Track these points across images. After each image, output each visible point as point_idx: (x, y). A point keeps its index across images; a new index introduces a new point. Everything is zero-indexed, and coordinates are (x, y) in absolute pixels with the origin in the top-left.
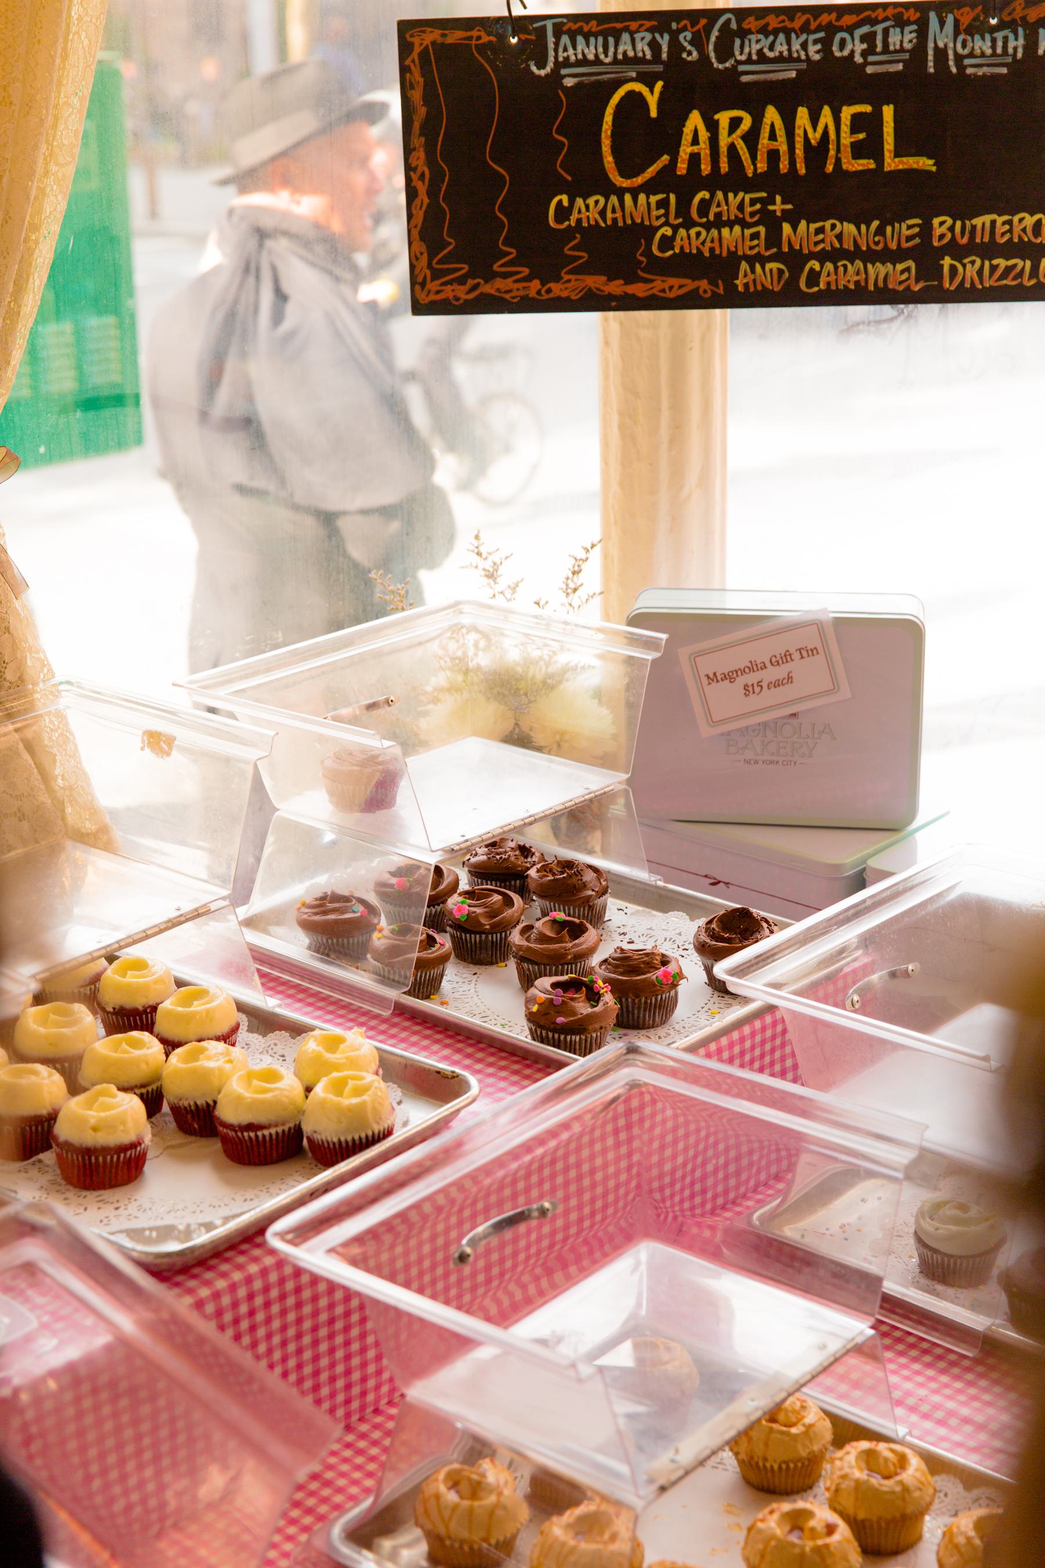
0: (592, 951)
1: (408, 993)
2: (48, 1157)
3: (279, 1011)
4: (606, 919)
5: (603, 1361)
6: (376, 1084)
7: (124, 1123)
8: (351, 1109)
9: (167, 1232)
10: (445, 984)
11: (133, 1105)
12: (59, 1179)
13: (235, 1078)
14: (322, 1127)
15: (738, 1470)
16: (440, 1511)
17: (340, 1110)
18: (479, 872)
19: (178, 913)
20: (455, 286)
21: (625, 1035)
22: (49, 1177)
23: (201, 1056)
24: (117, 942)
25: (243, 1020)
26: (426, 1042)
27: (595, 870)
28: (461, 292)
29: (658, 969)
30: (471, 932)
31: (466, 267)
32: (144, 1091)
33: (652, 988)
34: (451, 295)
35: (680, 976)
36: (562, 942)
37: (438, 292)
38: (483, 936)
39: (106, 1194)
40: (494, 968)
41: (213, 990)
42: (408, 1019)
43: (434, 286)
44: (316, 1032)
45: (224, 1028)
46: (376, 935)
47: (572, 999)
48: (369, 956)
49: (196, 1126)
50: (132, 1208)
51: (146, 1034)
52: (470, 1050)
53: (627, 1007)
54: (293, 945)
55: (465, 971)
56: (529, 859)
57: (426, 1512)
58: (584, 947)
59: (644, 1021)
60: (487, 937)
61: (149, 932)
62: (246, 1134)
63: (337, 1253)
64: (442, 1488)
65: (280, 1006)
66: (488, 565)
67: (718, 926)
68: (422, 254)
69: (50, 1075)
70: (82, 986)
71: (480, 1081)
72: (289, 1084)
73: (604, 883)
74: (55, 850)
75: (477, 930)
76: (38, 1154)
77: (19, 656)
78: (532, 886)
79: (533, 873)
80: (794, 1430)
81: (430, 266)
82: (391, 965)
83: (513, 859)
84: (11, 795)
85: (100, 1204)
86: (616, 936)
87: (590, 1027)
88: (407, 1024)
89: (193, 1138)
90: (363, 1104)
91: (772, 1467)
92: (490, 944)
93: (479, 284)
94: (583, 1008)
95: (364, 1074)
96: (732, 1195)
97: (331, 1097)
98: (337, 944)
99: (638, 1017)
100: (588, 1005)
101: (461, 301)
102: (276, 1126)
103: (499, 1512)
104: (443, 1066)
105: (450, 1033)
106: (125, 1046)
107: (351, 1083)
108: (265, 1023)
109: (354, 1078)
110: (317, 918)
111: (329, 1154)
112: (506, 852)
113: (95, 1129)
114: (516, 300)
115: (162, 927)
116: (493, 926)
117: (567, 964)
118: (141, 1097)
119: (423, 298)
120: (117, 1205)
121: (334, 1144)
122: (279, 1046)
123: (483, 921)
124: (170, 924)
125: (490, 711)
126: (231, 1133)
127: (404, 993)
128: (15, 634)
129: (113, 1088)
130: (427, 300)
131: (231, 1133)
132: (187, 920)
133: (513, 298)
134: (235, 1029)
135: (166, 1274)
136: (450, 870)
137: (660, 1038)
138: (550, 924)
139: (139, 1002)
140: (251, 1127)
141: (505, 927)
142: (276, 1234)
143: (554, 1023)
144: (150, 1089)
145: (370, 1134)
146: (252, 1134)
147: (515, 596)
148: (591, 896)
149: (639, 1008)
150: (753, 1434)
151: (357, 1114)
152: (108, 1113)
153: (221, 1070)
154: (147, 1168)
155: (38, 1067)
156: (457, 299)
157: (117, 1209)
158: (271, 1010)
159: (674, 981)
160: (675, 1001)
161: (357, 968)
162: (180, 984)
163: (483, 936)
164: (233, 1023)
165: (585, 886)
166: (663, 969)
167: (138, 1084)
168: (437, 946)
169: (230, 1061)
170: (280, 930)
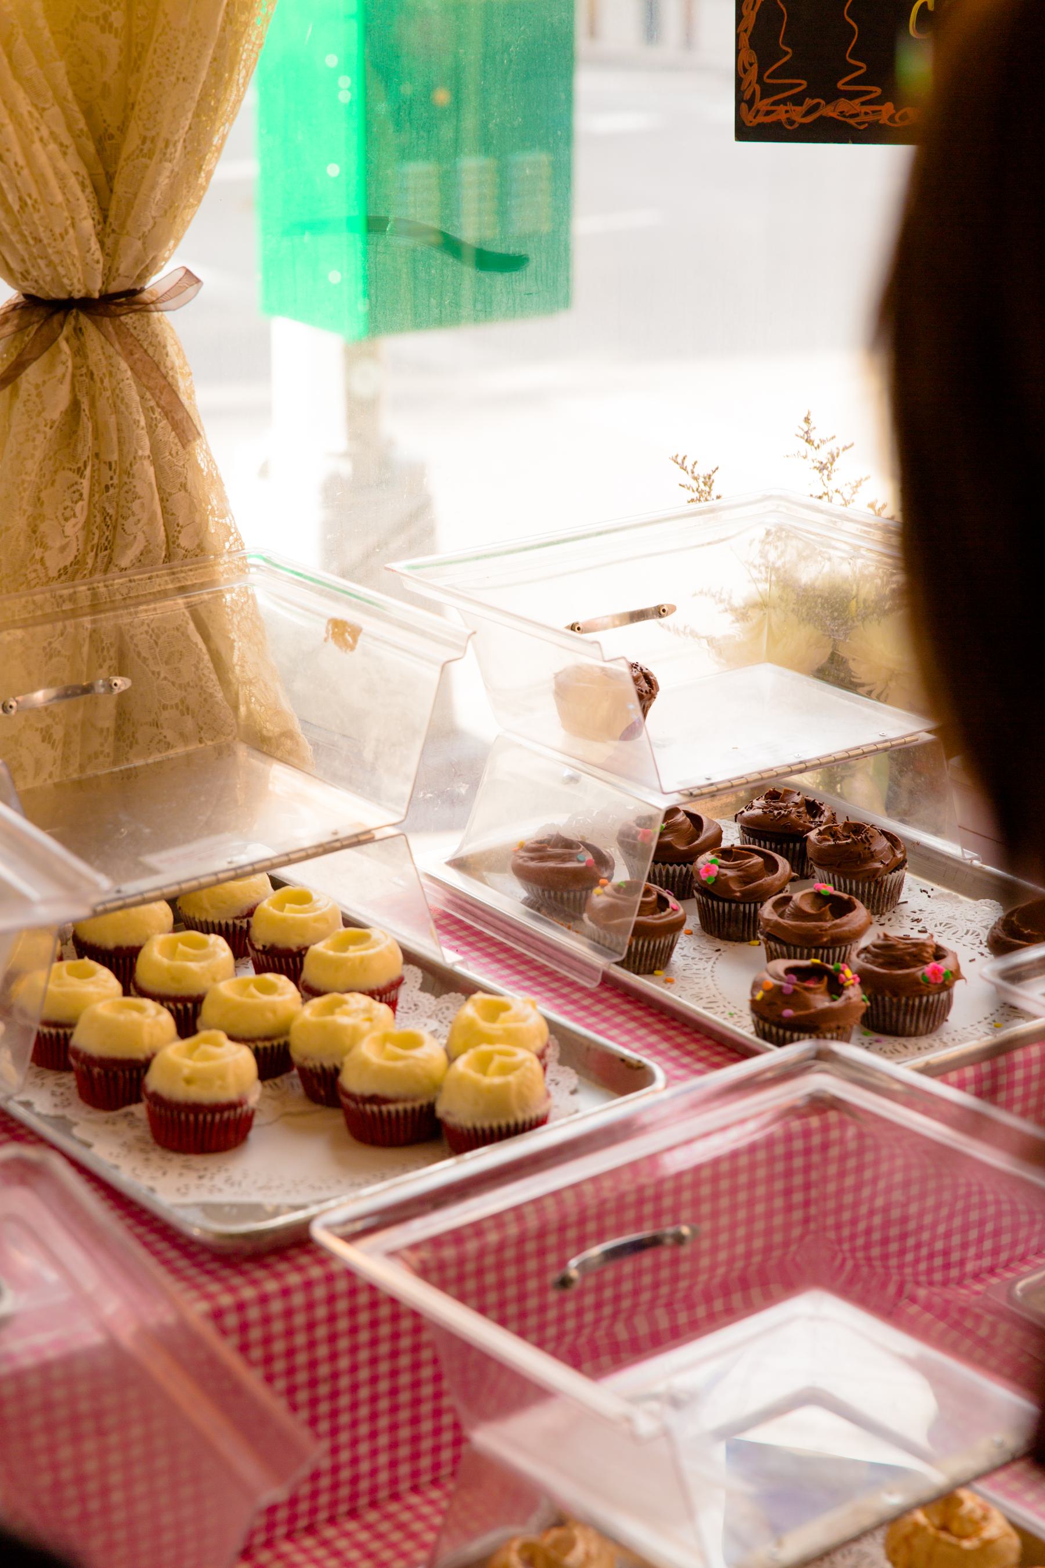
0: (858, 934)
1: (619, 964)
2: (139, 1110)
3: (460, 969)
4: (900, 901)
5: (758, 1435)
7: (222, 1077)
8: (492, 1090)
9: (255, 1210)
10: (676, 957)
11: (241, 1060)
12: (149, 1137)
14: (456, 1110)
17: (480, 1091)
18: (753, 829)
20: (790, 107)
21: (877, 1041)
22: (138, 1132)
23: (337, 1010)
24: (252, 864)
25: (414, 976)
27: (893, 839)
28: (797, 114)
29: (926, 963)
30: (719, 899)
31: (805, 83)
32: (261, 1045)
33: (916, 987)
34: (783, 117)
35: (956, 975)
36: (821, 920)
37: (768, 113)
38: (733, 906)
39: (196, 1160)
40: (744, 946)
42: (619, 996)
43: (763, 105)
44: (479, 996)
45: (381, 981)
46: (598, 890)
47: (807, 989)
48: (585, 916)
50: (219, 1180)
51: (284, 978)
52: (681, 1039)
53: (884, 1006)
54: (506, 897)
55: (707, 945)
56: (817, 820)
58: (846, 928)
59: (904, 1028)
60: (737, 907)
61: (293, 856)
65: (462, 963)
66: (823, 455)
67: (1018, 920)
68: (751, 65)
69: (159, 1013)
70: (237, 918)
71: (666, 1072)
73: (900, 856)
74: (223, 752)
75: (726, 897)
77: (197, 520)
78: (810, 851)
79: (813, 835)
80: (967, 1544)
81: (760, 80)
82: (606, 927)
83: (793, 816)
84: (173, 684)
85: (184, 1171)
86: (907, 923)
87: (823, 1026)
88: (616, 1001)
89: (318, 1107)
90: (506, 1087)
92: (741, 915)
93: (819, 104)
94: (821, 1002)
96: (1004, 1256)
97: (474, 1075)
98: (550, 897)
99: (897, 1021)
100: (827, 998)
101: (796, 126)
102: (405, 1100)
105: (665, 1017)
106: (253, 990)
107: (498, 1060)
108: (442, 982)
109: (501, 1053)
110: (533, 864)
111: (466, 1141)
112: (787, 807)
113: (188, 1081)
114: (862, 127)
115: (310, 852)
116: (744, 894)
117: (823, 948)
118: (257, 1053)
119: (751, 121)
120: (202, 1173)
122: (451, 1011)
123: (734, 886)
124: (320, 850)
125: (802, 637)
127: (617, 963)
128: (193, 492)
129: (222, 1036)
130: (756, 122)
131: (352, 1105)
132: (343, 847)
133: (860, 124)
134: (398, 983)
136: (711, 821)
137: (919, 1049)
138: (809, 900)
139: (293, 942)
140: (374, 1099)
141: (759, 897)
143: (780, 1016)
144: (275, 1043)
146: (375, 1108)
147: (855, 497)
148: (878, 869)
149: (898, 1009)
150: (916, 1542)
151: (498, 1098)
154: (253, 1134)
155: (148, 1003)
156: (791, 122)
157: (201, 1177)
158: (449, 967)
159: (946, 983)
160: (948, 1005)
161: (569, 928)
163: (733, 906)
164: (394, 976)
165: (872, 856)
166: (933, 964)
168: (669, 910)
169: (370, 1020)
170: (495, 877)
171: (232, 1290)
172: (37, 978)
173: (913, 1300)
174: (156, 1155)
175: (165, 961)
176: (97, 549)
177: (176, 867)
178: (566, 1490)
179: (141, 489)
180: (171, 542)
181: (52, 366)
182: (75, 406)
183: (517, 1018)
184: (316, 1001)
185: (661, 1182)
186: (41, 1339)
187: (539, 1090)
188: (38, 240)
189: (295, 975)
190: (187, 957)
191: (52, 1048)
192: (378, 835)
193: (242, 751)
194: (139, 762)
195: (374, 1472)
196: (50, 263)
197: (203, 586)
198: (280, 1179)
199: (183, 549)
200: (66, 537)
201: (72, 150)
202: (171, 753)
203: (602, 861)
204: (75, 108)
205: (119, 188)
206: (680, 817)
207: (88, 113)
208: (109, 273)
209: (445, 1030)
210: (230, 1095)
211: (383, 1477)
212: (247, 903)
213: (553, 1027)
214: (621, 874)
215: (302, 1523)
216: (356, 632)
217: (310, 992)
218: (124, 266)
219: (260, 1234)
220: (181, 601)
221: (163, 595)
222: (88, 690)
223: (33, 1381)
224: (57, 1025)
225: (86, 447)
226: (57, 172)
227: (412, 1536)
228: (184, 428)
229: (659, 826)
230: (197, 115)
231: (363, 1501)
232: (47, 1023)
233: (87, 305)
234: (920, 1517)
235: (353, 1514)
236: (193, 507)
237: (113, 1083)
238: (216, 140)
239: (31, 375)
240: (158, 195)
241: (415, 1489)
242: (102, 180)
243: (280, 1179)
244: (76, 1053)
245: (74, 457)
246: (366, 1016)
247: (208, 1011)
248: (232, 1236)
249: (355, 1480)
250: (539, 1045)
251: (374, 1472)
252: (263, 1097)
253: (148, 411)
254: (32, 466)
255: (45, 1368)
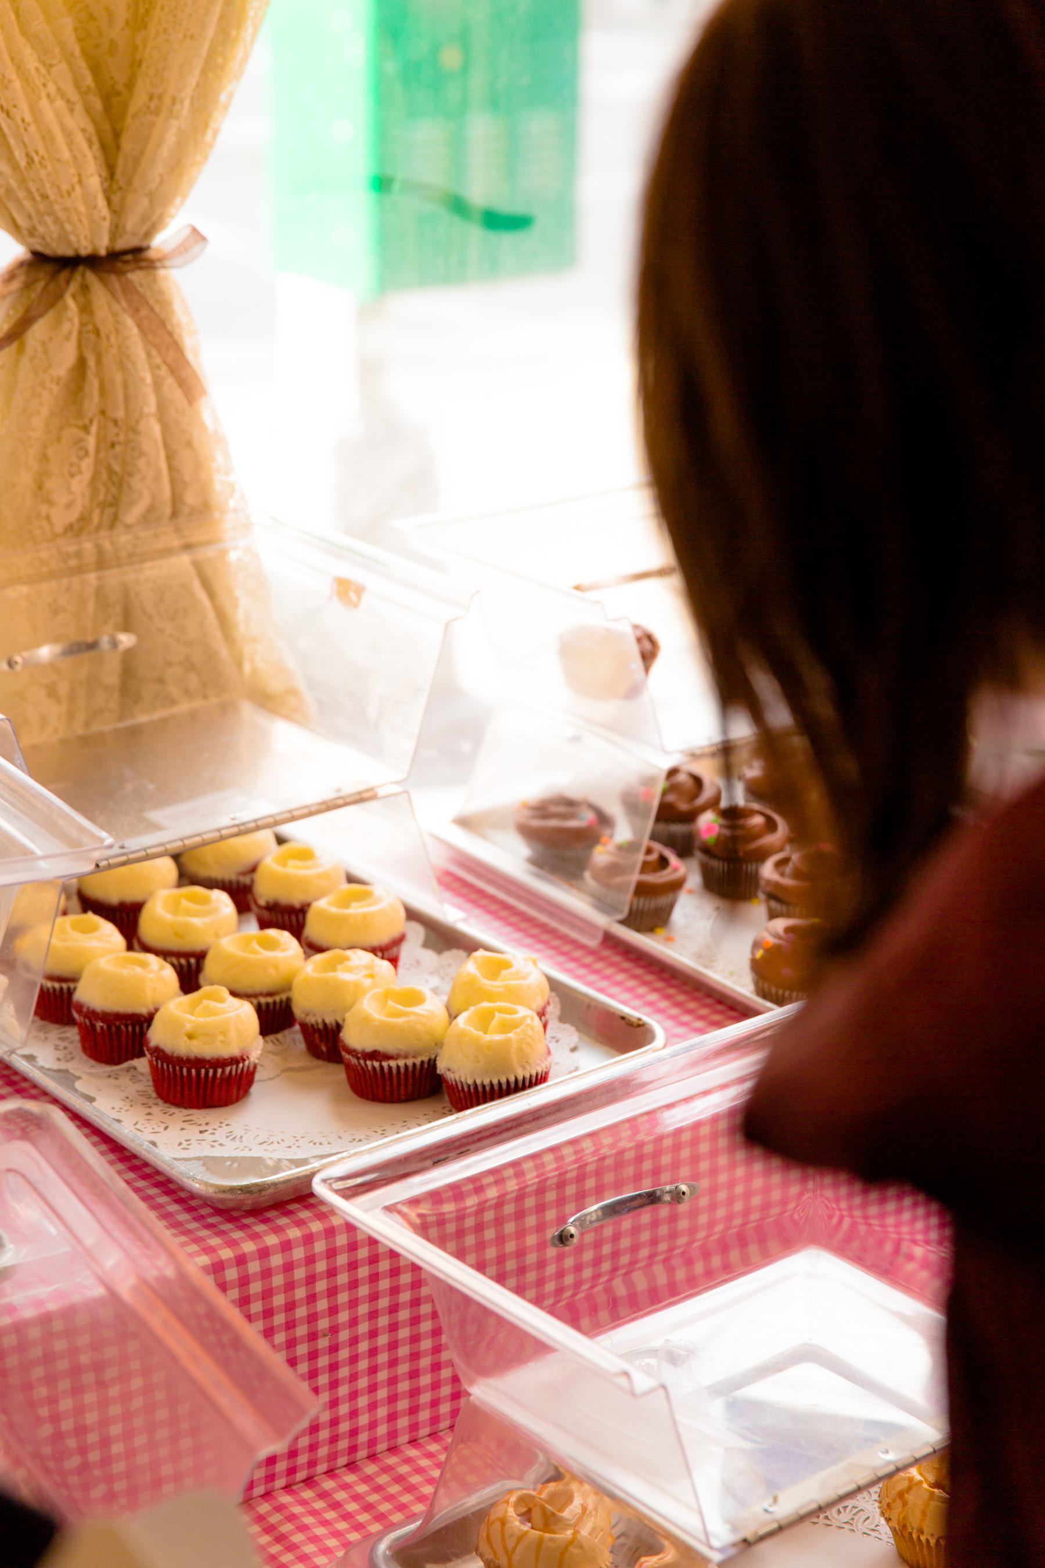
1: (622, 922)
2: (142, 1064)
6: (529, 1021)
7: (224, 1033)
8: (491, 1046)
11: (246, 1013)
13: (368, 996)
14: (457, 1067)
15: (892, 1541)
16: (503, 1539)
19: (337, 795)
22: (140, 1087)
23: (340, 967)
24: (255, 821)
25: (416, 933)
26: (632, 983)
32: (263, 1000)
39: (198, 1115)
41: (377, 890)
44: (480, 953)
45: (383, 938)
48: (587, 875)
49: (324, 1049)
50: (221, 1135)
51: (286, 934)
52: (681, 998)
54: (510, 856)
57: (488, 1538)
62: (369, 1063)
63: (399, 1212)
64: (511, 1512)
65: (464, 920)
69: (161, 968)
71: (666, 1030)
72: (432, 1007)
74: (227, 709)
76: (132, 1059)
82: (607, 886)
85: (185, 1125)
89: (320, 1063)
90: (507, 1042)
91: (928, 1541)
95: (519, 1008)
102: (406, 1057)
103: (573, 1550)
104: (626, 1010)
107: (498, 1017)
108: (444, 938)
109: (501, 1010)
113: (190, 1037)
115: (313, 809)
118: (259, 1010)
121: (469, 1086)
124: (323, 807)
126: (354, 1061)
129: (225, 992)
131: (354, 1061)
132: (346, 804)
134: (399, 941)
135: (235, 1214)
139: (296, 899)
140: (374, 1055)
142: (324, 1181)
144: (277, 999)
145: (512, 1079)
146: (376, 1064)
151: (499, 1055)
152: (208, 1019)
153: (357, 985)
154: (254, 1089)
155: (151, 958)
162: (351, 879)
167: (265, 990)
168: (669, 870)
171: (233, 1244)
172: (42, 932)
173: (910, 1257)
174: (159, 1109)
175: (169, 917)
176: (103, 505)
177: (180, 822)
178: (564, 1445)
179: (146, 446)
180: (176, 500)
181: (58, 322)
182: (81, 363)
183: (518, 976)
184: (318, 957)
185: (660, 1138)
186: (41, 1291)
187: (540, 1048)
188: (45, 197)
189: (297, 931)
190: (190, 913)
191: (56, 1004)
192: (381, 792)
193: (247, 710)
194: (143, 718)
195: (373, 1425)
196: (57, 220)
197: (208, 543)
198: (285, 1132)
199: (188, 508)
200: (72, 493)
201: (79, 108)
202: (176, 710)
203: (604, 820)
204: (82, 64)
205: (126, 144)
206: (682, 778)
207: (96, 69)
208: (116, 231)
209: (447, 988)
210: (231, 1050)
211: (382, 1430)
212: (248, 860)
213: (554, 985)
214: (623, 832)
215: (301, 1475)
216: (360, 590)
217: (313, 948)
218: (131, 223)
219: (261, 1188)
220: (185, 559)
221: (169, 552)
222: (93, 646)
223: (34, 1333)
224: (60, 979)
225: (92, 403)
226: (63, 129)
227: (410, 1489)
228: (185, 380)
229: (661, 785)
230: (204, 72)
231: (362, 1454)
232: (51, 978)
233: (92, 261)
234: (914, 1472)
235: (352, 1466)
236: (198, 465)
237: (116, 1038)
238: (223, 98)
239: (38, 331)
240: (165, 152)
241: (413, 1442)
242: (109, 136)
243: (285, 1132)
244: (79, 1008)
245: (80, 414)
246: (368, 972)
247: (210, 966)
248: (232, 1190)
249: (354, 1433)
250: (539, 1002)
251: (373, 1425)
252: (265, 1052)
253: (154, 368)
254: (38, 422)
255: (46, 1319)
